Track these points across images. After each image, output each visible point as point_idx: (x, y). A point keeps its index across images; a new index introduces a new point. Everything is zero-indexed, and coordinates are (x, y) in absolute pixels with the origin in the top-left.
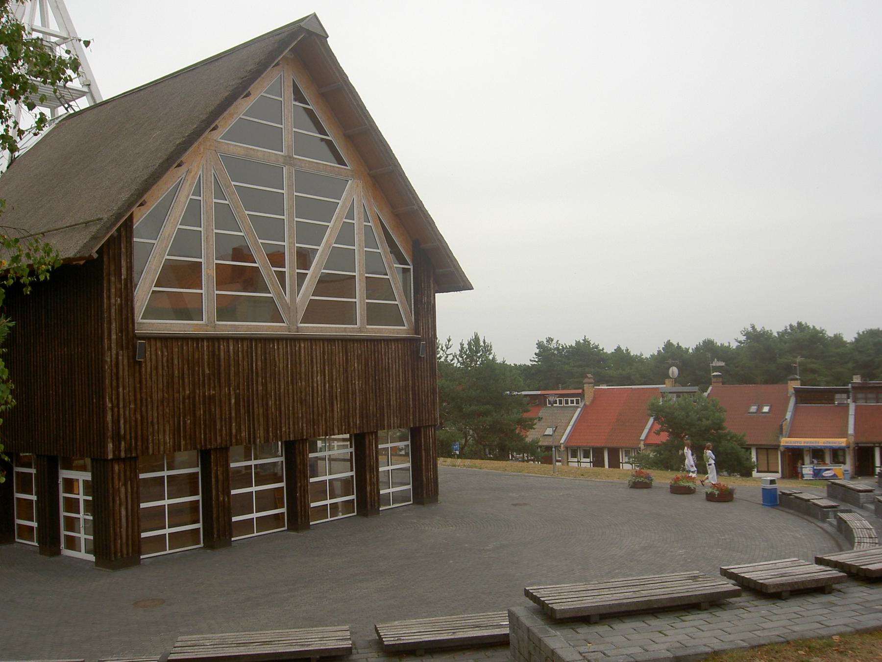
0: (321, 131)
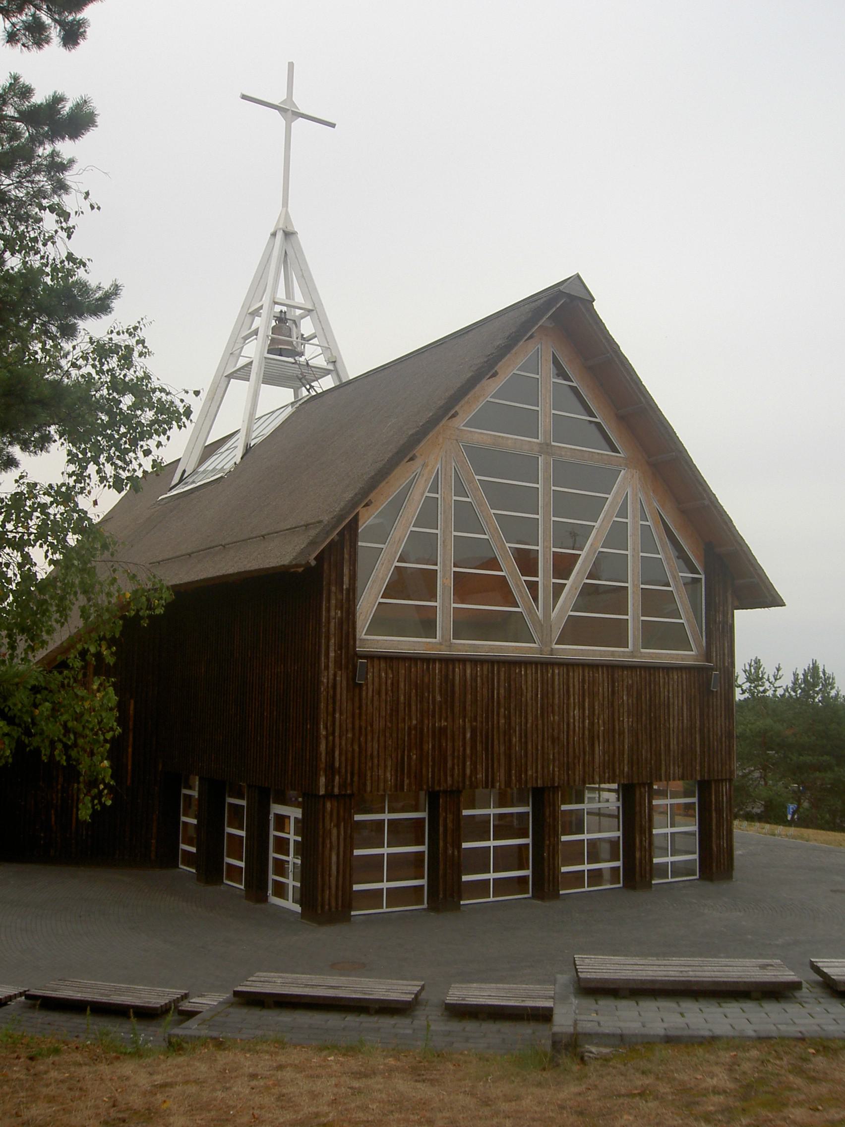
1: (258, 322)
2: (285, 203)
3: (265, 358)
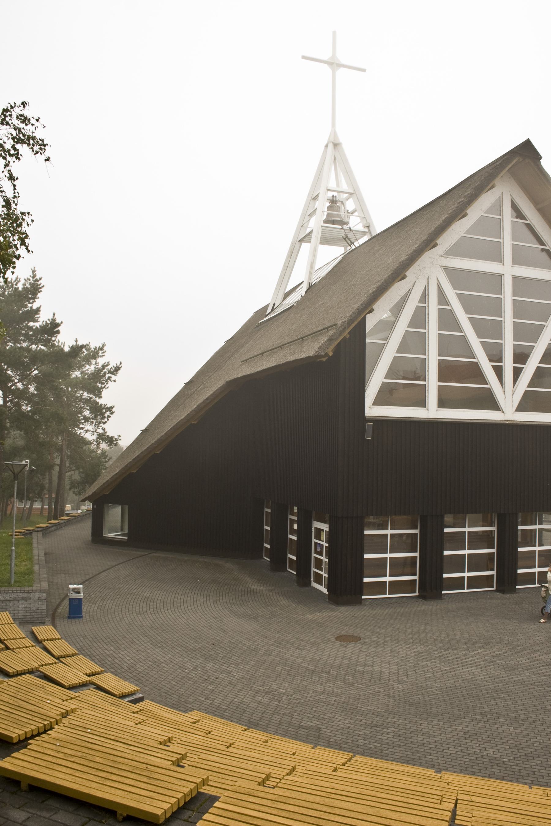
0: (542, 243)
1: (317, 204)
2: (333, 125)
3: (322, 226)
